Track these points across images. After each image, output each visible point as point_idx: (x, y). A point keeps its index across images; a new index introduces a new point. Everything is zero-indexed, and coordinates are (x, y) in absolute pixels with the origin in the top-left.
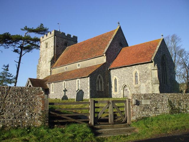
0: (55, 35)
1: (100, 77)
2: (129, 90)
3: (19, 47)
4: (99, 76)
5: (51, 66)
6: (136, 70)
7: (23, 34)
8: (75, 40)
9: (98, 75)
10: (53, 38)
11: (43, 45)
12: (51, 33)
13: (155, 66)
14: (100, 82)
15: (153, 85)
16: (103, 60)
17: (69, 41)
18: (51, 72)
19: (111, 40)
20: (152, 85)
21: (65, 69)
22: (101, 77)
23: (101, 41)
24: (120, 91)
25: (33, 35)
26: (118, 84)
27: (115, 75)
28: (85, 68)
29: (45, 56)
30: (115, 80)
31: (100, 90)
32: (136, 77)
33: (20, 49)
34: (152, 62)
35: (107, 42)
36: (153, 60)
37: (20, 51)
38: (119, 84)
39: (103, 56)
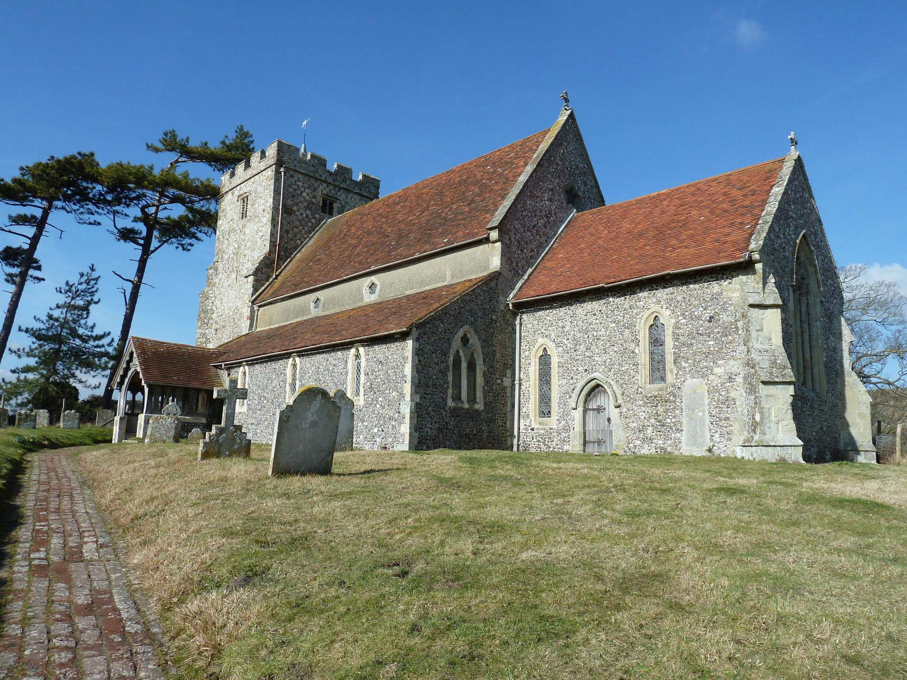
0: (279, 163)
1: (465, 340)
2: (614, 413)
3: (136, 220)
4: (460, 334)
5: (255, 289)
6: (654, 308)
8: (369, 189)
9: (458, 326)
10: (270, 173)
11: (228, 207)
12: (263, 154)
13: (765, 284)
14: (464, 365)
15: (763, 390)
16: (491, 258)
17: (342, 196)
18: (251, 318)
19: (529, 169)
20: (752, 390)
21: (312, 305)
22: (474, 340)
23: (481, 180)
24: (564, 416)
25: (199, 172)
27: (539, 337)
28: (401, 299)
29: (236, 254)
30: (545, 360)
31: (466, 406)
32: (656, 342)
33: (141, 227)
34: (746, 267)
35: (509, 182)
36: (756, 256)
37: (144, 234)
38: (562, 376)
39: (487, 240)
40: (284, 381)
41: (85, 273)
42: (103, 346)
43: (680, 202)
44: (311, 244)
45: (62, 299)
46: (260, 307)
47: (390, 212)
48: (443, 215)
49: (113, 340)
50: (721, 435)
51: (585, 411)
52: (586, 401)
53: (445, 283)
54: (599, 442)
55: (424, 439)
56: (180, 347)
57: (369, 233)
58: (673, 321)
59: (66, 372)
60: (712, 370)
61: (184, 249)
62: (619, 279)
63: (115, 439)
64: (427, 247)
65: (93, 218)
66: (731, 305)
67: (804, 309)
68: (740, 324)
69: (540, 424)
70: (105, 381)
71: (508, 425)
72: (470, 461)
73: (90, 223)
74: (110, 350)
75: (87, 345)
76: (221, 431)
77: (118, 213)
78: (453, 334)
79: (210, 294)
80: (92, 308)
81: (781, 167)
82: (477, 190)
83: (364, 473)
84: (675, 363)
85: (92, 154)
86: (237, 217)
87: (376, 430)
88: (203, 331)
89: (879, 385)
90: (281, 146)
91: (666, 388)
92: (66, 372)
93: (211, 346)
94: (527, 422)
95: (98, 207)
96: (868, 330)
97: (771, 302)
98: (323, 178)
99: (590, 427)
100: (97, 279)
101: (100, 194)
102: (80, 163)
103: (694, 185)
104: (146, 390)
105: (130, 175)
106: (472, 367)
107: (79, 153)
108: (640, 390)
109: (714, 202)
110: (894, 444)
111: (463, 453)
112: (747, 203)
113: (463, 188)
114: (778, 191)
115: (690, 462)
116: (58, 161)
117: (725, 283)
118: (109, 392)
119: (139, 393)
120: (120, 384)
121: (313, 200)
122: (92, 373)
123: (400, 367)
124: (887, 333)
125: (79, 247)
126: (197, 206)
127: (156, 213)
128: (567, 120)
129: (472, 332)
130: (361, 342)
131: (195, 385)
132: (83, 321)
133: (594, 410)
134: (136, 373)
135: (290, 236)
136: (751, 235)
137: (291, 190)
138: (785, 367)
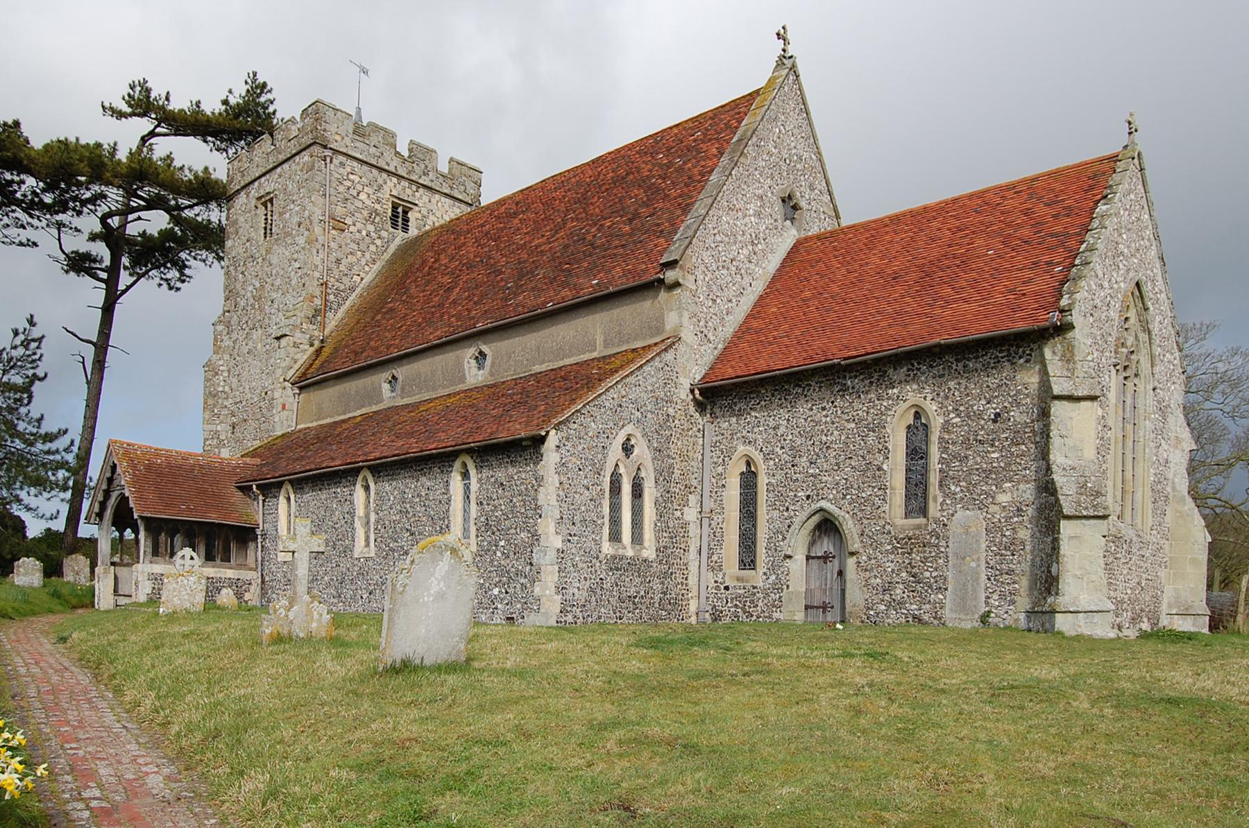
1: (627, 449)
3: (93, 237)
4: (621, 438)
7: (124, 137)
14: (626, 489)
22: (641, 451)
25: (192, 155)
28: (526, 379)
29: (258, 299)
31: (630, 553)
32: (916, 453)
33: (101, 250)
37: (107, 262)
38: (773, 506)
40: (352, 513)
41: (21, 330)
42: (57, 451)
43: (958, 223)
47: (502, 229)
48: (589, 238)
49: (72, 442)
50: (1002, 596)
53: (595, 355)
57: (470, 266)
60: (993, 498)
61: (171, 288)
62: (863, 351)
64: (566, 293)
65: (24, 235)
66: (1027, 395)
67: (1129, 401)
69: (738, 579)
70: (65, 509)
73: (21, 244)
74: (70, 458)
75: (33, 449)
77: (64, 226)
80: (37, 387)
82: (642, 195)
84: (941, 485)
85: (17, 124)
87: (496, 591)
88: (213, 427)
89: (1218, 510)
91: (926, 525)
95: (31, 216)
96: (1210, 422)
97: (1085, 393)
98: (392, 169)
100: (40, 340)
101: (34, 193)
105: (81, 161)
106: (637, 492)
108: (887, 527)
109: (1009, 225)
110: (1235, 604)
112: (1058, 229)
113: (619, 192)
119: (129, 530)
121: (377, 206)
122: (46, 495)
126: (188, 213)
127: (123, 226)
129: (639, 435)
130: (469, 451)
132: (23, 410)
133: (819, 558)
134: (123, 500)
135: (342, 268)
136: (1063, 283)
137: (341, 189)
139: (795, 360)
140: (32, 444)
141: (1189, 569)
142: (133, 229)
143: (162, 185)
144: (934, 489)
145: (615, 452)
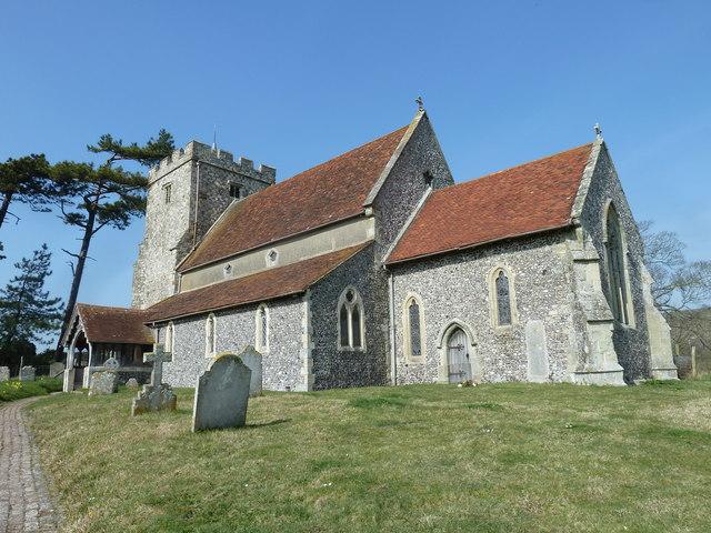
0: (195, 159)
2: (472, 350)
3: (80, 207)
4: (345, 292)
5: (179, 260)
7: (99, 161)
10: (188, 166)
11: (155, 194)
12: (182, 151)
14: (350, 316)
17: (245, 183)
19: (394, 158)
20: (580, 328)
24: (431, 354)
25: (131, 167)
26: (423, 326)
30: (414, 309)
32: (502, 292)
33: (85, 213)
34: (567, 231)
35: (378, 169)
38: (428, 322)
39: (363, 216)
40: (204, 335)
44: (221, 219)
45: (20, 273)
46: (183, 274)
51: (449, 348)
52: (448, 341)
54: (461, 374)
55: (320, 383)
56: (117, 310)
58: (514, 275)
59: (24, 332)
63: (65, 389)
64: (316, 222)
65: (44, 206)
68: (567, 275)
70: (57, 338)
71: (387, 363)
72: (360, 403)
74: (61, 312)
76: (151, 389)
78: (339, 292)
79: (140, 266)
80: (46, 279)
81: (590, 151)
83: (274, 423)
85: (43, 156)
86: (162, 202)
90: (196, 144)
92: (24, 332)
93: (143, 307)
94: (401, 363)
99: (453, 362)
101: (51, 187)
102: (33, 162)
103: (523, 166)
104: (90, 348)
107: (32, 155)
109: (540, 179)
111: (354, 392)
114: (590, 169)
115: (538, 391)
116: (15, 162)
117: (554, 246)
118: (60, 349)
120: (69, 343)
122: (47, 332)
123: (297, 322)
124: (672, 271)
125: (36, 230)
126: (129, 194)
128: (422, 119)
130: (266, 301)
131: (131, 340)
132: (38, 290)
134: (82, 334)
136: (572, 205)
138: (605, 309)
139: (435, 249)
140: (41, 306)
141: (661, 345)
142: (101, 202)
143: (117, 181)
144: (514, 310)
145: (342, 298)
